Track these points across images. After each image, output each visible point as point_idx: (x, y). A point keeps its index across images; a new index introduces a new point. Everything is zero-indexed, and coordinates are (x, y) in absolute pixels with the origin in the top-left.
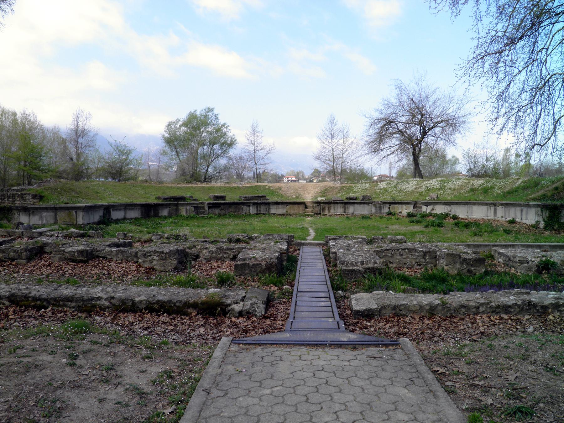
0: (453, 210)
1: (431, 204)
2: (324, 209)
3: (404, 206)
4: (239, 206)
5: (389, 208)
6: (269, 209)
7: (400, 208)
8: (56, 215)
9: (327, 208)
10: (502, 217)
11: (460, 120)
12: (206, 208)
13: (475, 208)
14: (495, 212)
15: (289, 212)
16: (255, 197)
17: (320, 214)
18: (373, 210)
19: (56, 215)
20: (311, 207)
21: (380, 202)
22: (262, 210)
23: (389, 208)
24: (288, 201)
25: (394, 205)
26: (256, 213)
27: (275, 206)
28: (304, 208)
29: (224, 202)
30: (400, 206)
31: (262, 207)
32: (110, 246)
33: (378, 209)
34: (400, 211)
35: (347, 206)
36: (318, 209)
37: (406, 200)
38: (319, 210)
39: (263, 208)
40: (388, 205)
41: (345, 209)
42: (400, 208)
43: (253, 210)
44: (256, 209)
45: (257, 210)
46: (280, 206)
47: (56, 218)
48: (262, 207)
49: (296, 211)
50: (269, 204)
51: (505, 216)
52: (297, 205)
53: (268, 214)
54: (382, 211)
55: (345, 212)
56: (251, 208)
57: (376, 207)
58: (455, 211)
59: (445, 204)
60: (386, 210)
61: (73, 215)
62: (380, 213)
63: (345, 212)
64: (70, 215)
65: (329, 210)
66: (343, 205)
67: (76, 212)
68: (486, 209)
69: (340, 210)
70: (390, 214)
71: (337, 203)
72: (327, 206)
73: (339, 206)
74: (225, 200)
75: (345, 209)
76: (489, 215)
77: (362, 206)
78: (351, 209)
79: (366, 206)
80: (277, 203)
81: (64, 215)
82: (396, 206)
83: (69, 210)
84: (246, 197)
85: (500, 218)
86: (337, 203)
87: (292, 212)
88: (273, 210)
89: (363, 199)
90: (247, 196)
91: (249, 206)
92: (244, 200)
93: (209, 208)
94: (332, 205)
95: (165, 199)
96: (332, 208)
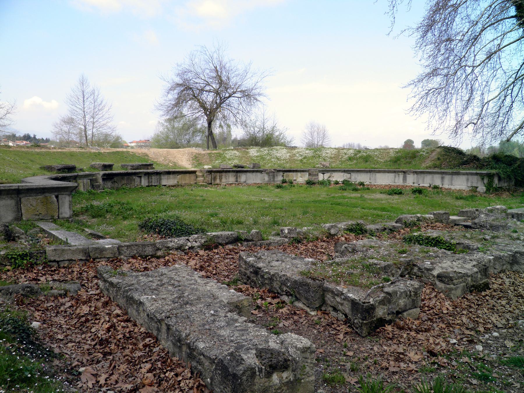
0: (353, 177)
1: (328, 171)
2: (215, 179)
3: (299, 174)
4: (131, 177)
5: (283, 176)
6: (160, 179)
7: (295, 176)
8: (18, 204)
9: (218, 177)
10: (414, 183)
11: (427, 78)
12: (100, 181)
13: (378, 175)
14: (405, 179)
15: (180, 183)
16: (143, 165)
17: (211, 184)
18: (266, 178)
19: (18, 204)
20: (200, 176)
21: (273, 171)
22: (153, 181)
23: (283, 176)
24: (178, 170)
25: (288, 173)
26: (147, 185)
27: (166, 176)
28: (195, 178)
29: (110, 172)
30: (295, 174)
31: (153, 177)
32: (467, 249)
33: (271, 177)
34: (295, 178)
35: (239, 174)
36: (209, 178)
37: (300, 167)
38: (210, 179)
39: (154, 178)
40: (281, 173)
41: (237, 178)
42: (295, 176)
43: (144, 182)
44: (147, 181)
45: (149, 182)
46: (171, 176)
47: (19, 209)
48: (153, 177)
49: (187, 182)
50: (158, 174)
51: (418, 182)
52: (188, 175)
53: (159, 186)
54: (276, 179)
55: (237, 181)
56: (143, 179)
57: (269, 176)
58: (355, 178)
59: (344, 171)
60: (279, 178)
61: (52, 203)
62: (274, 181)
63: (237, 181)
64: (46, 203)
65: (221, 179)
66: (235, 174)
67: (57, 197)
68: (394, 177)
69: (231, 178)
70: (284, 182)
71: (229, 171)
72: (218, 174)
73: (230, 174)
74: (111, 170)
75: (237, 178)
76: (396, 181)
77: (254, 174)
78: (243, 178)
79: (258, 174)
80: (169, 173)
81: (34, 203)
82: (290, 173)
83: (44, 193)
84: (133, 166)
85: (412, 184)
86: (229, 171)
87: (183, 183)
88: (166, 181)
89: (254, 167)
90: (134, 164)
91: (140, 177)
92: (131, 169)
93: (104, 180)
94: (224, 174)
95: (133, 168)
96: (223, 177)
